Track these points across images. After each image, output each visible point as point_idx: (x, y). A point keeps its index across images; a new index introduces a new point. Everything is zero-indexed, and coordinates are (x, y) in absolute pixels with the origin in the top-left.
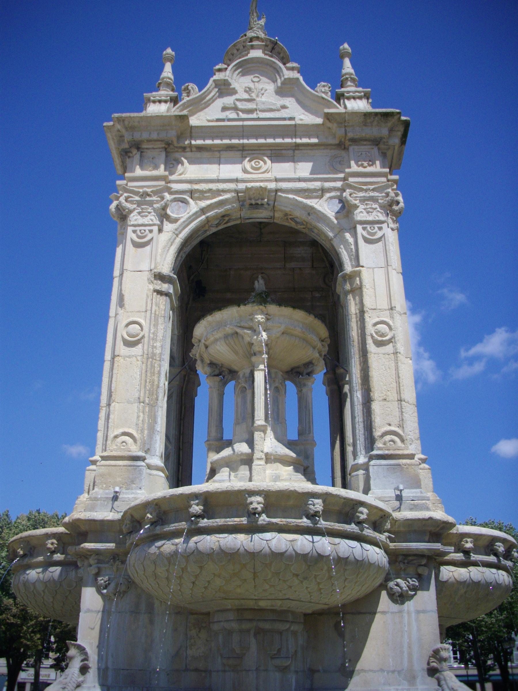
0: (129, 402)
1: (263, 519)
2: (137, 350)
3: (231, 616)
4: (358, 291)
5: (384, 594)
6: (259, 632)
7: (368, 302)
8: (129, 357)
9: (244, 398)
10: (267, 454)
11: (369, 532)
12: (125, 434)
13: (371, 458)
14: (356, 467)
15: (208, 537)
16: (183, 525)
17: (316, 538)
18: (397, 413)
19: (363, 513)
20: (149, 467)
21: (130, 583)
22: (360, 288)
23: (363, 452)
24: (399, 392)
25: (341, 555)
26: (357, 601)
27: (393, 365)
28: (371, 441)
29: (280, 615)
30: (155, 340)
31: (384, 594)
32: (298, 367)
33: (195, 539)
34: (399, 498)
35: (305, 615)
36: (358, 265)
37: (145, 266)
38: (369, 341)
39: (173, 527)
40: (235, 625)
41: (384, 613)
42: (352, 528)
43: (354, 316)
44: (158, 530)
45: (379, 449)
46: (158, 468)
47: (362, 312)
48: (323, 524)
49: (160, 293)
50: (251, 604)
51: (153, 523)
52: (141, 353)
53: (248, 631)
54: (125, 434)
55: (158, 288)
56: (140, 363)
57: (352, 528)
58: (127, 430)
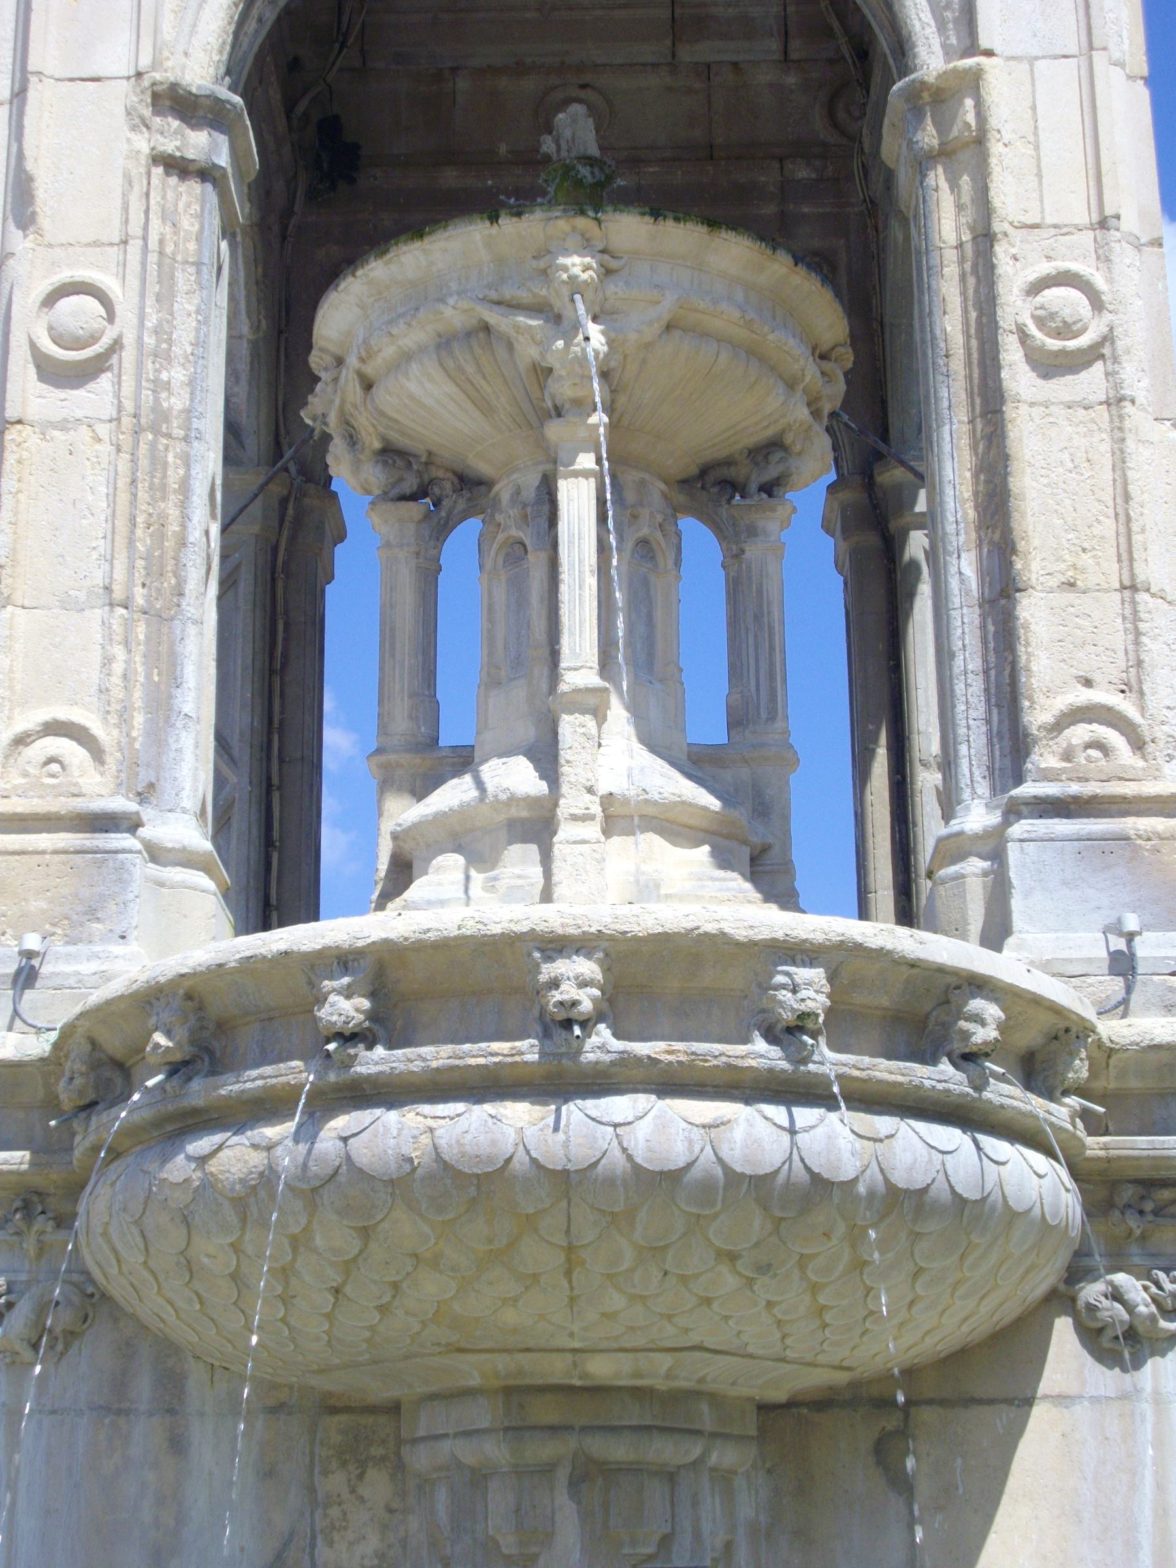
0: (68, 604)
1: (602, 1044)
2: (96, 398)
3: (482, 1415)
4: (971, 153)
5: (1063, 1329)
6: (587, 1475)
7: (1009, 195)
8: (63, 425)
9: (518, 586)
10: (608, 800)
11: (1006, 1093)
12: (55, 728)
13: (1014, 811)
14: (955, 848)
15: (392, 1117)
16: (296, 1072)
17: (805, 1115)
18: (1119, 639)
19: (985, 1022)
20: (155, 854)
21: (92, 1302)
22: (980, 141)
23: (983, 788)
24: (1127, 555)
25: (900, 1179)
26: (958, 1359)
27: (1104, 447)
28: (1012, 747)
29: (668, 1409)
30: (163, 356)
31: (1063, 1329)
32: (728, 462)
33: (341, 1123)
34: (1123, 965)
35: (765, 1408)
36: (972, 47)
37: (116, 57)
38: (1012, 354)
39: (256, 1079)
40: (496, 1451)
41: (1062, 1400)
42: (943, 1076)
43: (951, 255)
44: (199, 1092)
45: (1048, 776)
46: (188, 859)
47: (984, 238)
48: (828, 1061)
49: (177, 167)
50: (556, 1369)
51: (179, 1069)
52: (109, 411)
53: (548, 1470)
54: (55, 728)
55: (169, 146)
56: (105, 449)
57: (943, 1076)
58: (63, 713)
